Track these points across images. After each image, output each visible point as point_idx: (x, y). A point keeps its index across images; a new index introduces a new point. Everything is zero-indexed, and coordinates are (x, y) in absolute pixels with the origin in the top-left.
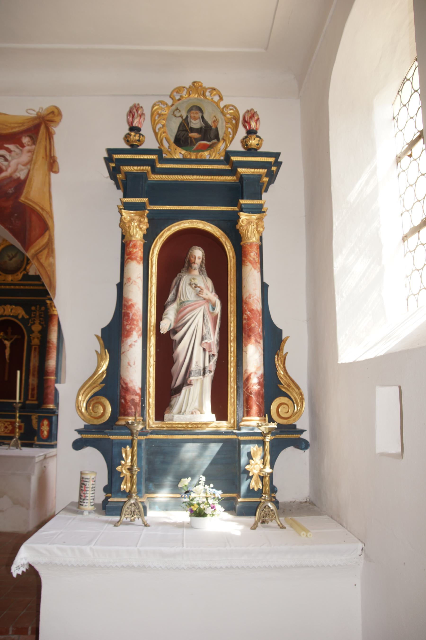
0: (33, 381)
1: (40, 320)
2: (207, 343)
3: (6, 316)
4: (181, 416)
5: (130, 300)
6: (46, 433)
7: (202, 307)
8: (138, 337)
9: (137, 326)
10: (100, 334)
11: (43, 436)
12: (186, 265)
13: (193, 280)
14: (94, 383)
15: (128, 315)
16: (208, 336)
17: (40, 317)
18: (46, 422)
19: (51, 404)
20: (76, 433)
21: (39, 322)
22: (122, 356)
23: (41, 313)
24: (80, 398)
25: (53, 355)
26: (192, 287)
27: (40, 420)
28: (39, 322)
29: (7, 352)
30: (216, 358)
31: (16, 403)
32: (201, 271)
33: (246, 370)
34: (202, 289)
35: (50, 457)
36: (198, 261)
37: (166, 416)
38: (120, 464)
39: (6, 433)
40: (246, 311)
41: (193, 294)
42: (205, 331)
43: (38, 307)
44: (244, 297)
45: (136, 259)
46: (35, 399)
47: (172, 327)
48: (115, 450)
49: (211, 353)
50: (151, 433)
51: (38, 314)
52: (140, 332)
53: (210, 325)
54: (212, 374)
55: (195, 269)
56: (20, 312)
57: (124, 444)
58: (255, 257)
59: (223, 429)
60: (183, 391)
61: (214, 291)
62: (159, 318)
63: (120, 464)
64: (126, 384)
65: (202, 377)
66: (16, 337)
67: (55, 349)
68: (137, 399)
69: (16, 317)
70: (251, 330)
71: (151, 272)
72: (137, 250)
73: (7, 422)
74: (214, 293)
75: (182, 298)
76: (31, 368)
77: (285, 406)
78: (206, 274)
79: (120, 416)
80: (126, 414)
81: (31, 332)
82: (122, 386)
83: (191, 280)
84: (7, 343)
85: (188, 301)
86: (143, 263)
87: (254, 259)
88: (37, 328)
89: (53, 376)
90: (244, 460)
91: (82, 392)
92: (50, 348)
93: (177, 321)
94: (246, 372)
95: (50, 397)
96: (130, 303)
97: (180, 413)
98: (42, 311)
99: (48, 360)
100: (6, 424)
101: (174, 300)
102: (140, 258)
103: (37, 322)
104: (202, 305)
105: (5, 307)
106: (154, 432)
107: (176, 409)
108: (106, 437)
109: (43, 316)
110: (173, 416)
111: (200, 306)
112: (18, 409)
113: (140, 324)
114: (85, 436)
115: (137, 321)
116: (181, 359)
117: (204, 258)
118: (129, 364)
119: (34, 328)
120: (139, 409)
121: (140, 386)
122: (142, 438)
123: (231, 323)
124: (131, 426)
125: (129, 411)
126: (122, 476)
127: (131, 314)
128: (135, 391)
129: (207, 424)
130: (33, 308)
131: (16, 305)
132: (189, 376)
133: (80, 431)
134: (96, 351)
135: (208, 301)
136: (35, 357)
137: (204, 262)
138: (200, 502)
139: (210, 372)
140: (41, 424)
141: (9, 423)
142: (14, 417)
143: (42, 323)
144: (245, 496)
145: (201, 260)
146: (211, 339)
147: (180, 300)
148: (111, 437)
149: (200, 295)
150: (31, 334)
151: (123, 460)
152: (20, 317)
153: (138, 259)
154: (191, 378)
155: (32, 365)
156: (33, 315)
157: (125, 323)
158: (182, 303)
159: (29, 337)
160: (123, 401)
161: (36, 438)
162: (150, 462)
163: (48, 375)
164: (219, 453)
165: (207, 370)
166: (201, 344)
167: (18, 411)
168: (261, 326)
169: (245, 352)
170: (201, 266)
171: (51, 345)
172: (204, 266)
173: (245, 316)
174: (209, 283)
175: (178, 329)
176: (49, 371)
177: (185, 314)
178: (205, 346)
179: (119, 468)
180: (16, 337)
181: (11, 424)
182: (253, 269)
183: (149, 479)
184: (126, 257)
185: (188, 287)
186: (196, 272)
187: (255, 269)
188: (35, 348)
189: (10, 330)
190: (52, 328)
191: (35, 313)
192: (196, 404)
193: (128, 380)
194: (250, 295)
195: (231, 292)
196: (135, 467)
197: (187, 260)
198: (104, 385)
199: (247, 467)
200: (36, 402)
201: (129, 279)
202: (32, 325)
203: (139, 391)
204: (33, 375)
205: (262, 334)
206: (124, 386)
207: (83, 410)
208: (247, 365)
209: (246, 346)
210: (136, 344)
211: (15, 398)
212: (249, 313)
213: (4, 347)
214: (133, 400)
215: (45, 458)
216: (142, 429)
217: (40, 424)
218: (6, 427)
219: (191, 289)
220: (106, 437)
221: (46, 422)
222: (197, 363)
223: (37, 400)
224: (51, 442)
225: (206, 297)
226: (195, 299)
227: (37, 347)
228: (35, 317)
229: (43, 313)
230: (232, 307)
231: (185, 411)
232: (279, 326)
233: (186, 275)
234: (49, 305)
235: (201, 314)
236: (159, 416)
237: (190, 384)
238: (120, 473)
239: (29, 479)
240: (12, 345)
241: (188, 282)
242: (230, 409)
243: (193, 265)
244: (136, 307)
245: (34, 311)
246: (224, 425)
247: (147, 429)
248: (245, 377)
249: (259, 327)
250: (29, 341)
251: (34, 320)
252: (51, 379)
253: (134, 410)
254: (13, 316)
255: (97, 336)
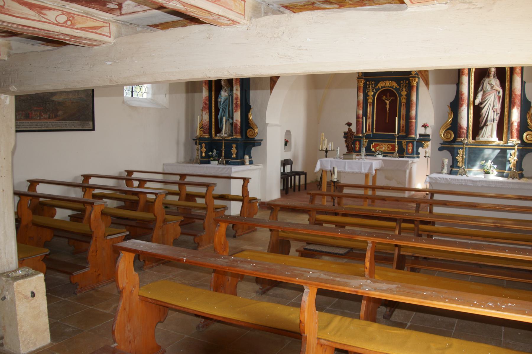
0: (403, 122)
1: (406, 89)
2: (495, 109)
3: (386, 87)
4: (483, 138)
5: (462, 92)
6: (410, 151)
7: (494, 93)
8: (466, 107)
9: (465, 102)
10: (449, 105)
11: (409, 152)
12: (487, 74)
13: (490, 81)
14: (447, 124)
15: (461, 98)
16: (496, 106)
17: (406, 87)
18: (410, 145)
19: (414, 135)
20: (440, 144)
21: (405, 89)
22: (459, 114)
23: (406, 84)
24: (441, 131)
25: (414, 108)
26: (489, 84)
27: (408, 143)
28: (405, 89)
29: (388, 107)
30: (499, 115)
31: (395, 134)
32: (494, 76)
33: (512, 120)
34: (494, 86)
35: (413, 163)
36: (493, 73)
37: (477, 138)
38: (457, 156)
39: (388, 150)
40: (513, 95)
41: (490, 87)
42: (494, 103)
43: (371, 82)
44: (513, 89)
45: (465, 74)
46: (404, 132)
47: (480, 102)
48: (455, 151)
49: (497, 113)
50: (470, 145)
51: (404, 85)
52: (467, 105)
53: (497, 101)
54: (497, 121)
55: (491, 76)
56: (394, 84)
57: (459, 148)
58: (518, 71)
59: (501, 144)
60: (484, 128)
61: (500, 85)
62: (475, 98)
63: (457, 156)
64: (460, 125)
65: (492, 123)
66: (392, 98)
67: (415, 105)
68: (465, 131)
69: (392, 87)
70: (515, 103)
71: (471, 91)
72: (465, 70)
73: (388, 145)
74: (499, 87)
75: (485, 89)
76: (402, 116)
77: (530, 135)
78: (496, 77)
79: (458, 138)
80: (460, 137)
81: (401, 95)
82: (459, 126)
83: (489, 82)
84: (388, 102)
85: (487, 91)
86: (468, 76)
87: (518, 72)
88: (404, 93)
89: (414, 120)
90: (509, 155)
91: (88, 124)
92: (412, 104)
93: (482, 99)
94: (512, 121)
95: (413, 131)
96: (462, 93)
97: (482, 137)
98: (407, 84)
99: (411, 111)
100: (389, 146)
101: (481, 90)
102: (467, 74)
103: (404, 90)
104: (494, 92)
105: (386, 82)
106: (471, 145)
107: (481, 135)
108: (452, 146)
109: (407, 86)
110: (479, 138)
111: (493, 93)
112: (397, 137)
113: (467, 101)
114: (443, 146)
115: (465, 100)
116: (484, 115)
117: (496, 71)
118: (462, 118)
119: (402, 93)
120: (466, 135)
121: (466, 126)
122: (467, 146)
123: (507, 99)
124: (463, 141)
125: (462, 136)
126: (458, 161)
127: (463, 98)
128: (464, 128)
129: (494, 142)
130: (402, 82)
131: (392, 81)
132: (487, 122)
133: (441, 144)
134: (448, 112)
135: (497, 90)
136: (403, 109)
137: (496, 72)
138: (488, 169)
139: (496, 120)
140: (408, 145)
141: (390, 145)
142: (395, 142)
143: (407, 90)
144: (508, 171)
145: (494, 72)
146: (497, 107)
147: (484, 90)
148: (454, 146)
149: (493, 88)
150: (401, 96)
151: (459, 154)
152: (394, 87)
153: (466, 74)
154: (488, 123)
155: (402, 114)
156: (401, 86)
157: (460, 101)
158: (484, 92)
159: (400, 98)
160: (459, 132)
161: (405, 153)
162: (469, 157)
163: (412, 120)
164: (499, 153)
165: (495, 120)
166: (492, 109)
167: (396, 139)
168: (520, 101)
169: (370, 174)
170: (494, 74)
171: (413, 103)
172: (495, 74)
173: (512, 97)
174: (498, 82)
175: (483, 103)
176: (412, 117)
177: (486, 97)
178: (495, 110)
179: (457, 158)
180: (392, 98)
181: (391, 146)
182: (517, 77)
183: (469, 163)
184: (461, 74)
185: (488, 85)
186: (492, 77)
187: (518, 76)
188: (403, 105)
189: (388, 95)
190: (413, 93)
191: (403, 85)
192: (490, 134)
193: (461, 124)
194: (515, 88)
195: (507, 86)
196: (464, 156)
197: (488, 72)
198: (450, 126)
199: (509, 159)
200: (405, 134)
201: (462, 83)
202: (401, 91)
203: (466, 128)
204: (403, 119)
205: (520, 105)
206: (460, 126)
207: (442, 136)
208: (512, 118)
209: (512, 110)
210: (465, 109)
211: (395, 132)
212: (514, 96)
213: (386, 104)
214: (463, 132)
215: (412, 163)
216: (467, 143)
217: (407, 145)
218: (388, 147)
219: (489, 86)
220: (452, 146)
221: (410, 145)
222: (490, 117)
223: (405, 133)
224: (413, 155)
225: (496, 89)
226: (491, 90)
227: (405, 104)
228: (403, 87)
229: (407, 84)
230: (507, 92)
231: (485, 136)
232: (530, 100)
233: (487, 79)
234: (411, 80)
235: (493, 96)
236: (474, 138)
237: (487, 126)
238: (457, 159)
239: (406, 171)
240: (389, 102)
241: (488, 82)
242: (504, 136)
243: (490, 75)
244: (465, 95)
245: (402, 84)
246: (501, 143)
247: (469, 143)
248: (511, 123)
249: (519, 101)
250: (400, 101)
251: (403, 89)
252: (413, 121)
253: (463, 136)
254: (390, 87)
255: (448, 106)
